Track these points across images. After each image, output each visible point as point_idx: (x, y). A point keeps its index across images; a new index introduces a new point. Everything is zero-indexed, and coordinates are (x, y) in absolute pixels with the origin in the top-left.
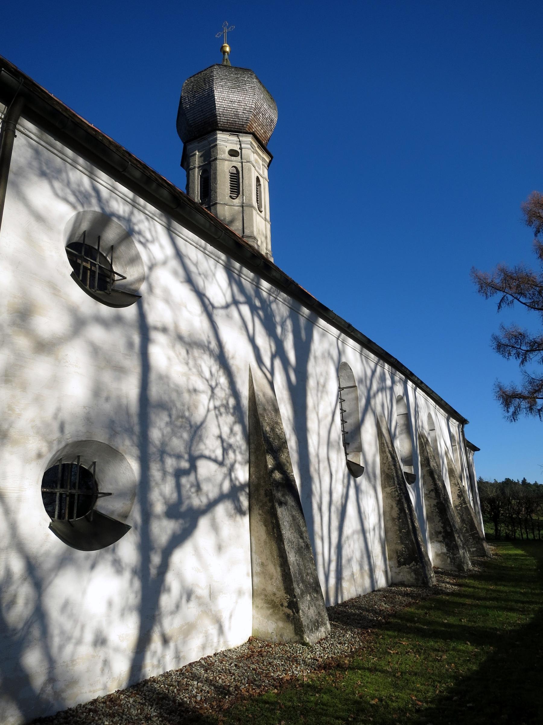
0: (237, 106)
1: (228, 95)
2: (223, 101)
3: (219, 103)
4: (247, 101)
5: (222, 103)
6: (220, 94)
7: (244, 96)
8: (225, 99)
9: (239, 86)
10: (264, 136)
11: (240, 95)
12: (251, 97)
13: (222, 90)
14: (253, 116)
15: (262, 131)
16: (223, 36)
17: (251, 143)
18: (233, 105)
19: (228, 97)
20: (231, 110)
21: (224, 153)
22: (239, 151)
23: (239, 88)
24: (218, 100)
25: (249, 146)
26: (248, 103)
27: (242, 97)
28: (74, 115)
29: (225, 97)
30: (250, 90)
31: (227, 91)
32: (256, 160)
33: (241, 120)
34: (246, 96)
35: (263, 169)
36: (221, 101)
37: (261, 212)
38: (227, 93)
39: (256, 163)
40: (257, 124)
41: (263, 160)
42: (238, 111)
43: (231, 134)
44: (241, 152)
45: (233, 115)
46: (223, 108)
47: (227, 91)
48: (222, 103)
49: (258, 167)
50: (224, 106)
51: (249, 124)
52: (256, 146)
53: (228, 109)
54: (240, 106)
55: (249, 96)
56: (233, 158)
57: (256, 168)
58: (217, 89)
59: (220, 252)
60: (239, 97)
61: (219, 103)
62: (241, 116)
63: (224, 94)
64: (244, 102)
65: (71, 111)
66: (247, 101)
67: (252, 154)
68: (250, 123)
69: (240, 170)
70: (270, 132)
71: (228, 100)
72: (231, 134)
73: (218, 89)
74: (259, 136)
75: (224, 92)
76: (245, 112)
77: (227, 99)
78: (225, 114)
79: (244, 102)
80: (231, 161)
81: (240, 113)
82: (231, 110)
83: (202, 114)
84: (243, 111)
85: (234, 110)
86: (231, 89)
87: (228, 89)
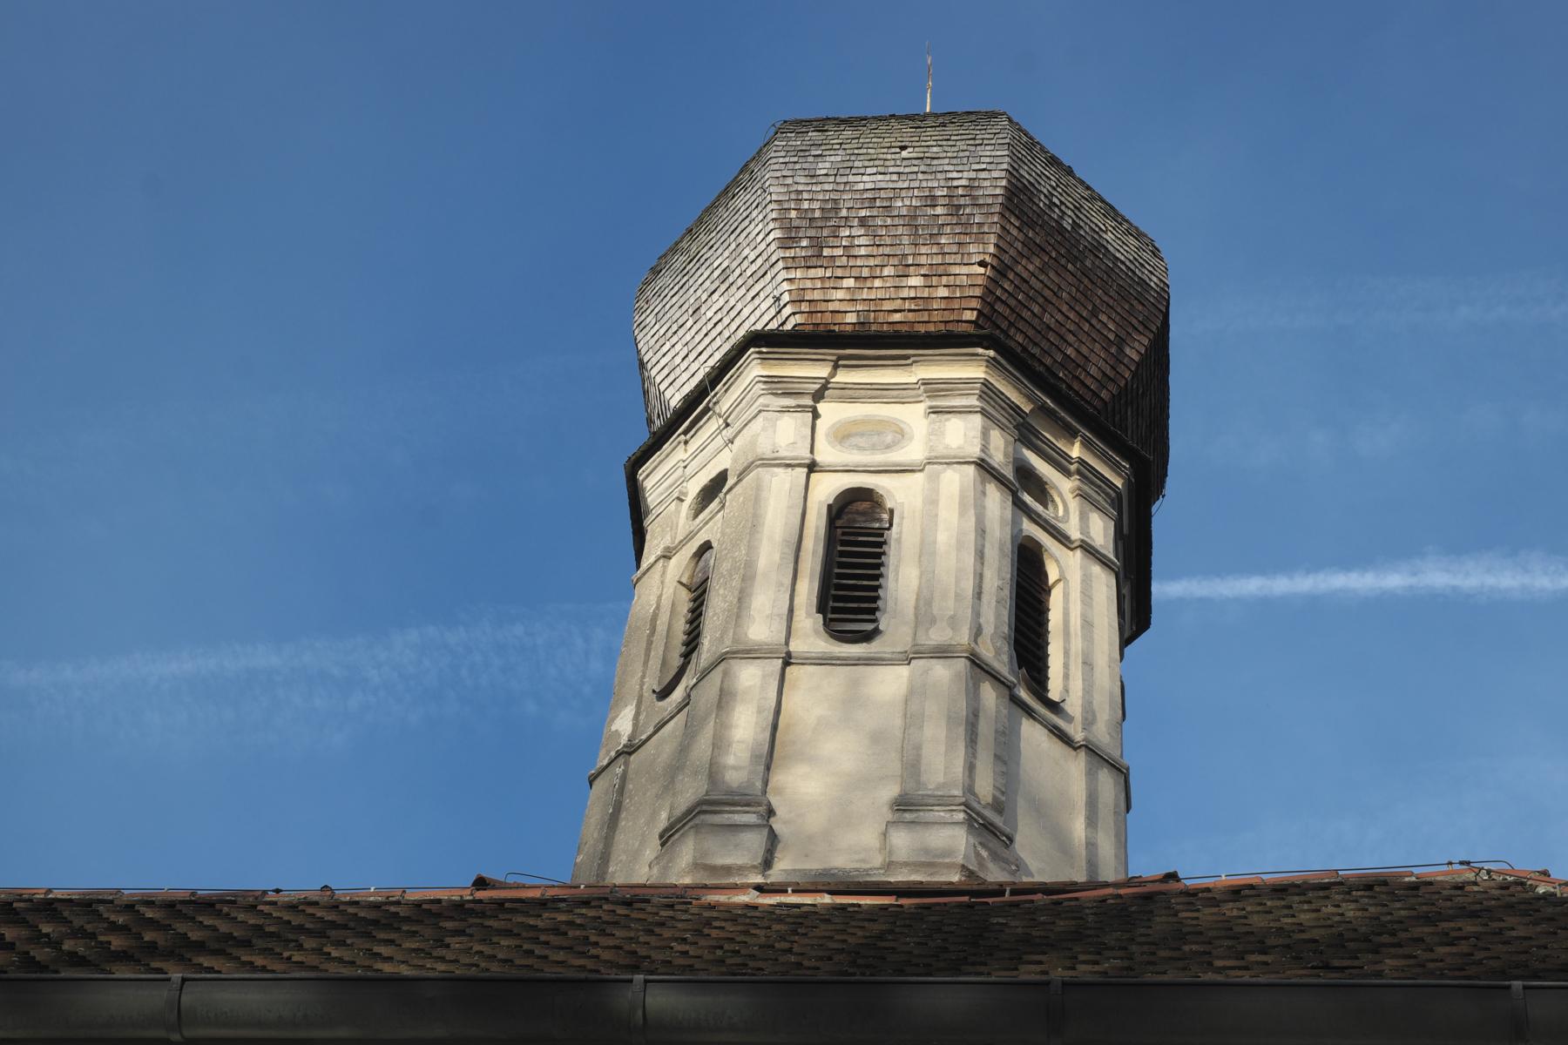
10: (943, 292)
40: (850, 283)
43: (685, 433)
74: (911, 317)
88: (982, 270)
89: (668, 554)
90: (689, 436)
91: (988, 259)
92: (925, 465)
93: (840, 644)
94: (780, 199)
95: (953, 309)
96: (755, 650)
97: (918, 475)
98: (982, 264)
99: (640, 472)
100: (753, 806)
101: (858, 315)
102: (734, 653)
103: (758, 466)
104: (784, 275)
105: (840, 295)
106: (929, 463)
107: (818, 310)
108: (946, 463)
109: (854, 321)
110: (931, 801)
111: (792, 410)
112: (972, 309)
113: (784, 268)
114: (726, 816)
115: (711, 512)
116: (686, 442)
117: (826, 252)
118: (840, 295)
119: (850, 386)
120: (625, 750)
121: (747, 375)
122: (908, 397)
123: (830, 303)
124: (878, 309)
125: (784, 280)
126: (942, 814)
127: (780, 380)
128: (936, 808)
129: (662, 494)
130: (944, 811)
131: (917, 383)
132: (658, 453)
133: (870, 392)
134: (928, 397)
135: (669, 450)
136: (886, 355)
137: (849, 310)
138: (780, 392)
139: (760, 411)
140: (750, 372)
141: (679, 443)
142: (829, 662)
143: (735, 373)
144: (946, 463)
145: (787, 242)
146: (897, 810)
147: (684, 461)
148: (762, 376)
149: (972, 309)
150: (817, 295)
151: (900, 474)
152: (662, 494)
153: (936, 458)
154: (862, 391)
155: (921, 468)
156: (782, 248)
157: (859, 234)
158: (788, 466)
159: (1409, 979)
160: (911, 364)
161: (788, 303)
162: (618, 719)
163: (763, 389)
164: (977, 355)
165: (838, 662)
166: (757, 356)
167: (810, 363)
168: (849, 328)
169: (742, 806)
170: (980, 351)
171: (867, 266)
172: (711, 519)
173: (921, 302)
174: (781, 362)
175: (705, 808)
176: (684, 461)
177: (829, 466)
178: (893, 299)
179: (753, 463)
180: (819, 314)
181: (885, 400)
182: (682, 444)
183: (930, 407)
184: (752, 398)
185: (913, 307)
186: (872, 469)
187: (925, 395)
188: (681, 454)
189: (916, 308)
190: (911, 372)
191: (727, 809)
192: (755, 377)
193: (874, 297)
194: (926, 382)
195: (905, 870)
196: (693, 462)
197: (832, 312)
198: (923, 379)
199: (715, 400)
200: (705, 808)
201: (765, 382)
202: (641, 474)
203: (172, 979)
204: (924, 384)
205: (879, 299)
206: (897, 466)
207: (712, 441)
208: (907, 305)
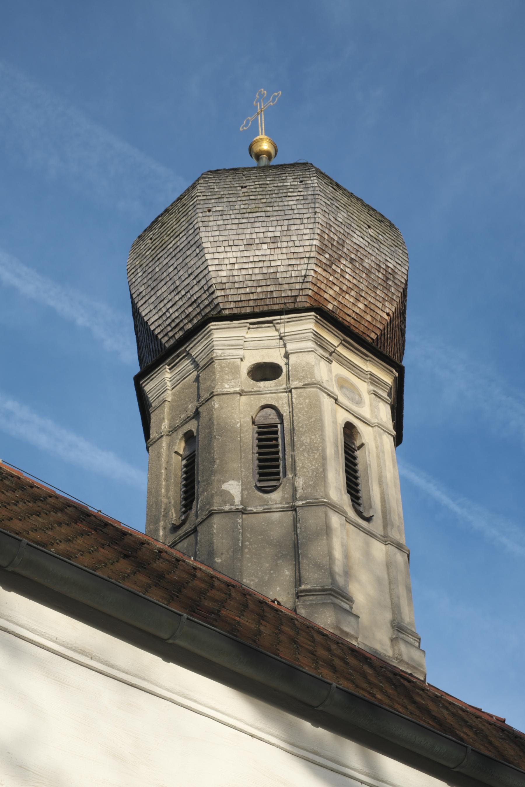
0: (268, 252)
1: (239, 231)
2: (228, 249)
3: (217, 256)
4: (296, 232)
5: (225, 255)
6: (217, 233)
7: (286, 222)
8: (231, 243)
9: (269, 204)
10: (369, 318)
11: (275, 223)
12: (305, 221)
13: (221, 222)
14: (319, 270)
15: (361, 306)
16: (256, 121)
17: (317, 335)
18: (258, 253)
19: (240, 237)
20: (251, 265)
21: (235, 371)
22: (281, 362)
23: (268, 209)
24: (211, 250)
25: (310, 345)
26: (300, 238)
27: (279, 228)
28: (395, 667)
29: (233, 237)
30: (300, 206)
31: (236, 221)
32: (342, 383)
33: (287, 287)
34: (291, 222)
35: (371, 404)
36: (222, 249)
37: (368, 520)
38: (234, 227)
39: (341, 387)
40: (337, 289)
41: (374, 380)
42: (273, 264)
43: (251, 324)
44: (287, 364)
45: (259, 277)
46: (229, 267)
47: (236, 221)
48: (225, 255)
49: (352, 400)
50: (233, 261)
51: (310, 293)
52: (335, 342)
53: (246, 266)
54: (278, 251)
55: (299, 222)
56: (263, 385)
57: (342, 399)
58: (206, 224)
59: (321, 731)
60: (271, 229)
61: (217, 256)
62: (285, 275)
63: (227, 232)
64: (288, 239)
65: (399, 668)
66: (296, 232)
67: (323, 364)
68: (315, 289)
69: (285, 410)
70: (387, 304)
71: (240, 242)
72: (251, 324)
73: (211, 224)
74: (352, 322)
75: (229, 227)
76: (293, 262)
77: (236, 242)
78: (237, 279)
79: (288, 239)
80: (259, 393)
81: (280, 269)
82: (251, 265)
83: (177, 298)
84: (287, 262)
85: (261, 264)
86: (247, 215)
87: (239, 216)
88: (386, 317)
89: (242, 393)
90: (252, 326)
91: (391, 313)
92: (375, 426)
93: (358, 517)
94: (323, 224)
95: (369, 329)
96: (337, 508)
97: (370, 428)
98: (388, 314)
99: (213, 323)
100: (349, 601)
101: (333, 307)
102: (329, 504)
103: (317, 388)
104: (314, 267)
105: (331, 292)
106: (378, 426)
107: (320, 294)
108: (384, 430)
109: (331, 309)
110: (408, 631)
111: (325, 358)
112: (376, 334)
113: (315, 264)
114: (339, 601)
115: (277, 390)
116: (249, 328)
117: (334, 267)
118: (331, 292)
119: (342, 356)
120: (243, 511)
121: (302, 324)
122: (361, 376)
123: (325, 294)
124: (342, 309)
125: (313, 269)
126: (412, 640)
127: (320, 337)
128: (410, 636)
129: (225, 346)
130: (413, 639)
131: (367, 372)
132: (229, 322)
133: (348, 364)
134: (370, 382)
135: (237, 325)
136: (349, 342)
137: (331, 302)
138: (319, 343)
139: (312, 351)
140: (308, 323)
141: (246, 326)
142: (359, 527)
143: (298, 317)
144: (384, 430)
145: (321, 251)
146: (397, 630)
147: (245, 338)
148: (314, 330)
149: (376, 334)
150: (323, 286)
151: (358, 420)
152: (225, 346)
153: (381, 425)
154: (346, 362)
155: (373, 426)
156: (317, 252)
157: (349, 266)
158: (329, 395)
159: (4, 529)
160: (367, 361)
161: (310, 282)
162: (226, 483)
163: (313, 338)
164: (392, 372)
165: (362, 529)
166: (315, 318)
167: (333, 335)
168: (369, 339)
169: (345, 599)
170: (394, 371)
171: (346, 285)
172: (275, 393)
173: (359, 317)
174: (323, 328)
175: (333, 593)
176: (245, 338)
177: (341, 403)
178: (350, 308)
179: (315, 384)
180: (319, 296)
181: (353, 372)
182: (247, 328)
183: (374, 391)
184: (305, 338)
185: (355, 318)
186: (356, 415)
187: (369, 380)
188: (242, 333)
189: (356, 319)
190: (366, 364)
191: (341, 598)
192: (311, 329)
193: (343, 302)
194: (372, 374)
195: (406, 666)
196: (251, 342)
197: (325, 298)
198: (371, 372)
199: (279, 321)
200: (333, 593)
201: (314, 334)
202: (212, 325)
203: (23, 541)
204: (370, 374)
205: (345, 305)
206: (364, 419)
207: (268, 340)
208: (353, 315)
